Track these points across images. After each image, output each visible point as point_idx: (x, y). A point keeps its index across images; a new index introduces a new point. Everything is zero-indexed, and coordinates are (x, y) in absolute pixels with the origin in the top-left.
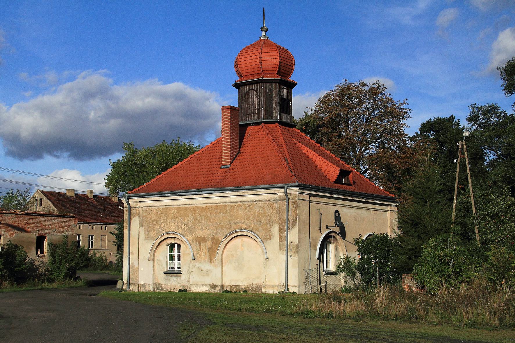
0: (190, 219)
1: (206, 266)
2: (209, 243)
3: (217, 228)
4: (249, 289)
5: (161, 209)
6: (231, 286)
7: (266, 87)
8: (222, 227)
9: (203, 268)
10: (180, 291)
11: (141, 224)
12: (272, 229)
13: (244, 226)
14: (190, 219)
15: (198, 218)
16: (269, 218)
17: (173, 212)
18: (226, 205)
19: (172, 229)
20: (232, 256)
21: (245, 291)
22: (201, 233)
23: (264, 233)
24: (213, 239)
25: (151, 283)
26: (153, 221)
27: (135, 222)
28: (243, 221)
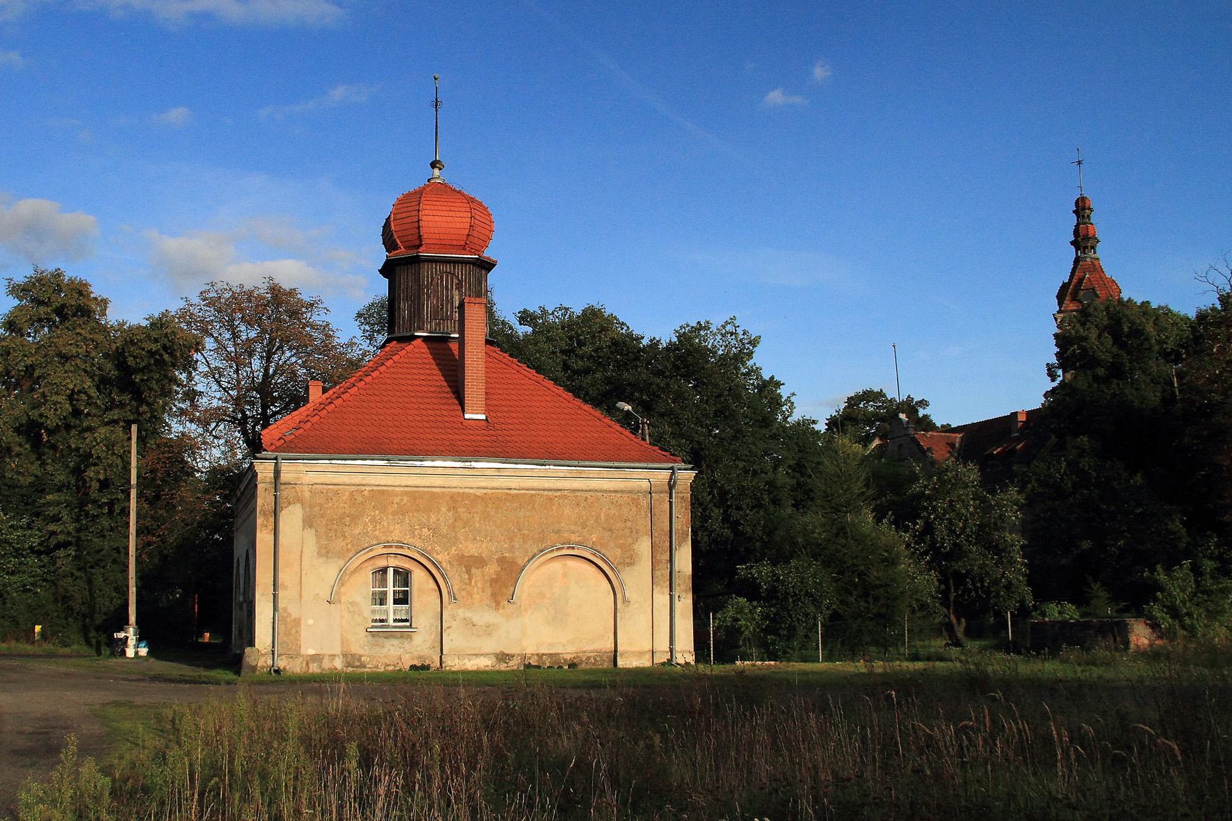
0: (443, 516)
1: (485, 616)
2: (492, 569)
3: (511, 539)
4: (582, 662)
5: (366, 493)
6: (540, 656)
7: (423, 273)
8: (525, 539)
9: (475, 619)
10: (413, 667)
11: (308, 522)
12: (636, 547)
13: (574, 538)
14: (443, 516)
15: (465, 516)
16: (629, 524)
17: (397, 500)
18: (533, 495)
19: (396, 536)
20: (542, 595)
21: (572, 665)
22: (472, 549)
23: (618, 552)
24: (502, 561)
25: (338, 651)
26: (342, 518)
27: (291, 519)
28: (573, 527)
